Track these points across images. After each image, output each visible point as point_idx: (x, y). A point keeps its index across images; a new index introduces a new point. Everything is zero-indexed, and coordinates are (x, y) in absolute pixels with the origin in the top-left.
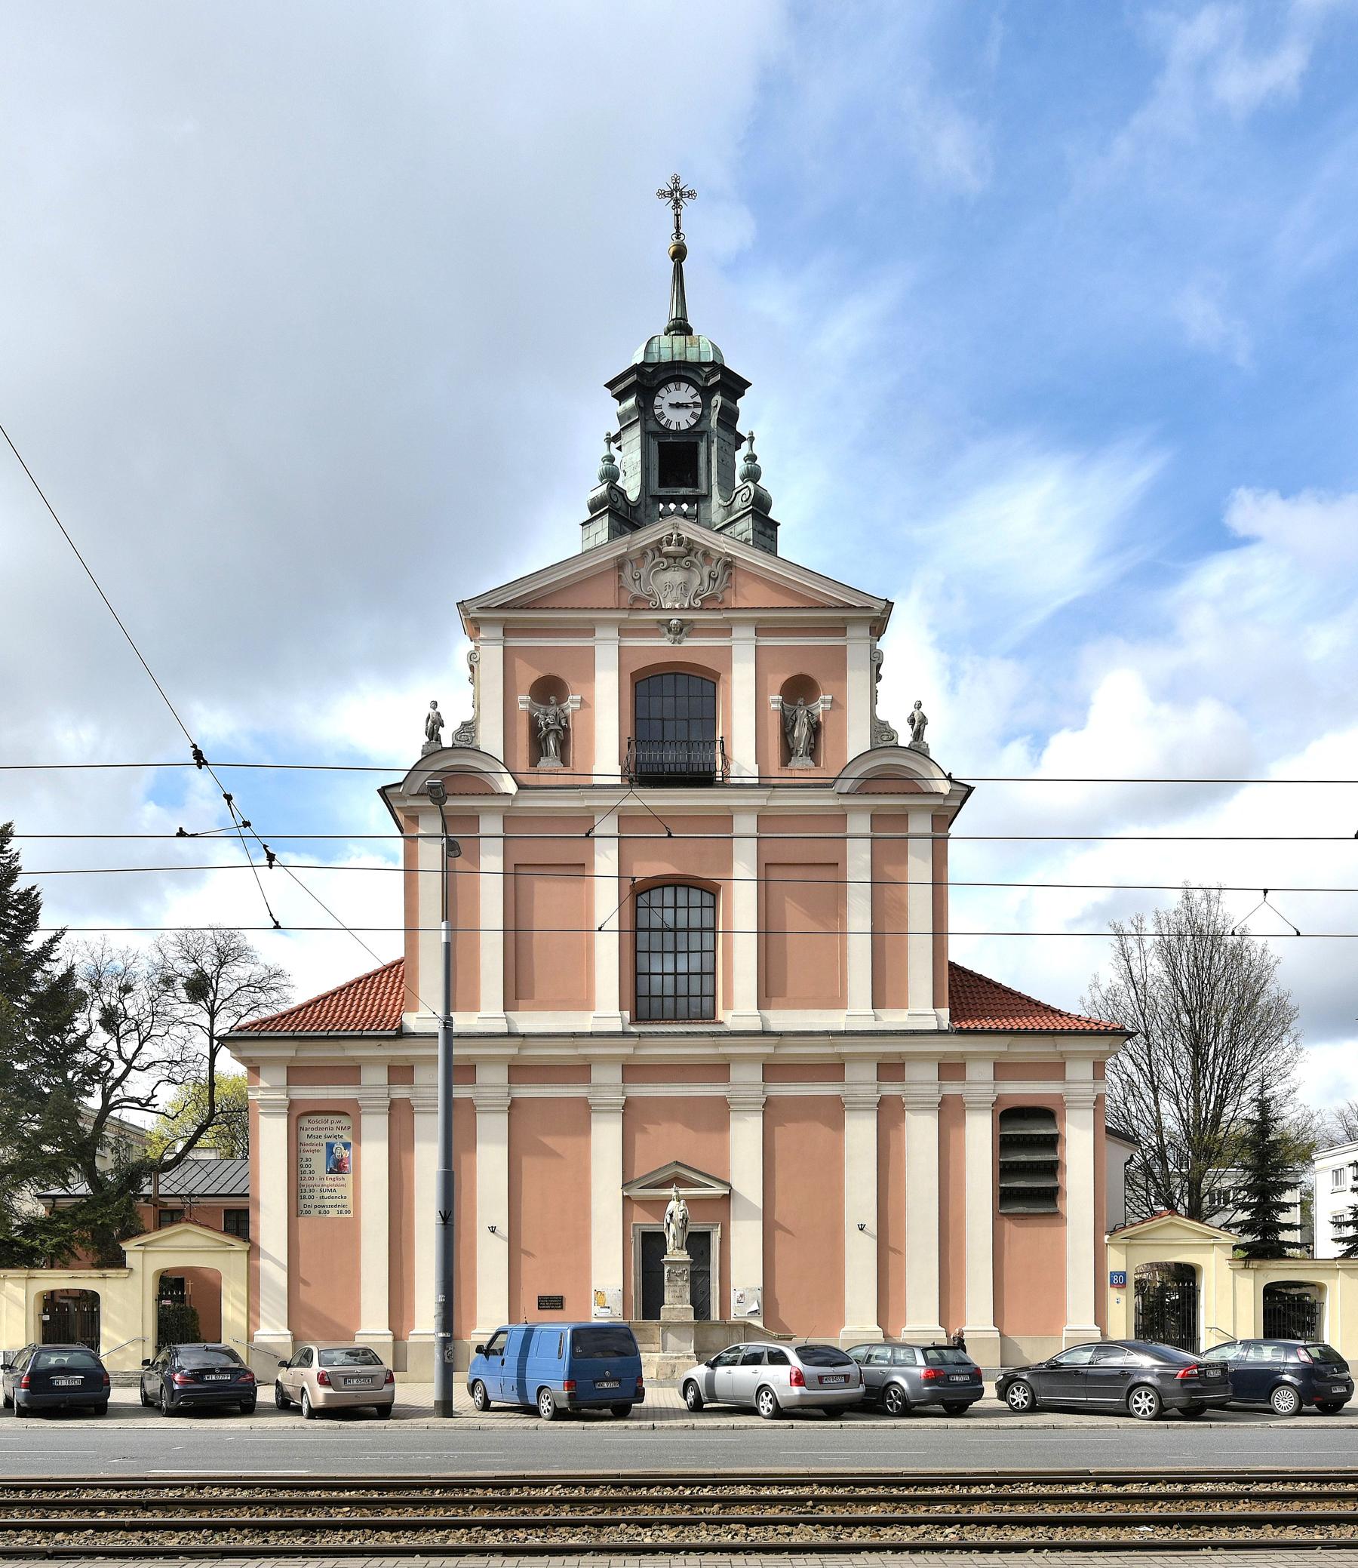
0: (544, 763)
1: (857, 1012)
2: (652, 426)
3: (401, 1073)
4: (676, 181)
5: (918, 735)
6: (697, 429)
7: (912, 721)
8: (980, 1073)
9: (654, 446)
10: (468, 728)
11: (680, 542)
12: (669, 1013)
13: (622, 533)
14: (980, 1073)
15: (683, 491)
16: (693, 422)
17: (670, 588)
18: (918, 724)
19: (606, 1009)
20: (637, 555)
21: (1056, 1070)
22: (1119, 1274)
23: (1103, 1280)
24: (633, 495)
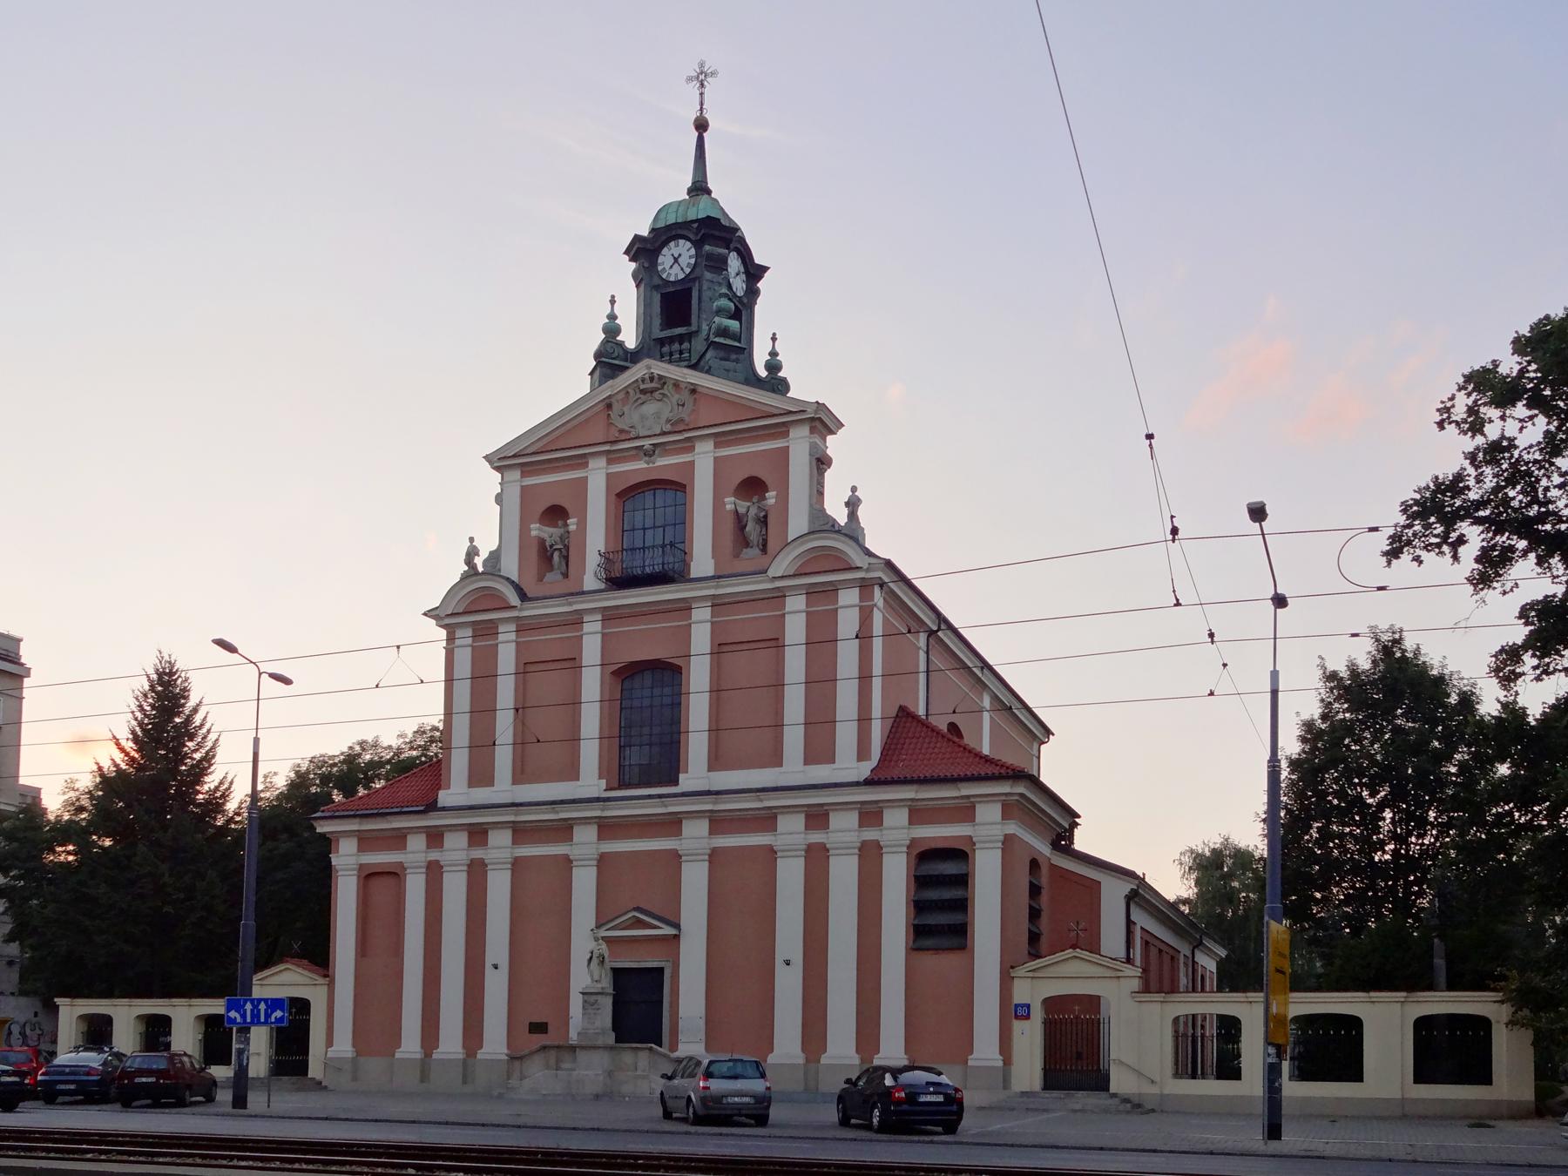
0: (549, 577)
1: (793, 769)
2: (656, 281)
3: (435, 837)
4: (702, 65)
5: (853, 516)
7: (847, 504)
8: (896, 819)
9: (657, 298)
10: (495, 557)
12: (636, 781)
14: (896, 819)
17: (651, 416)
18: (853, 504)
19: (591, 782)
20: (621, 396)
21: (965, 812)
22: (1022, 1006)
23: (1012, 1012)
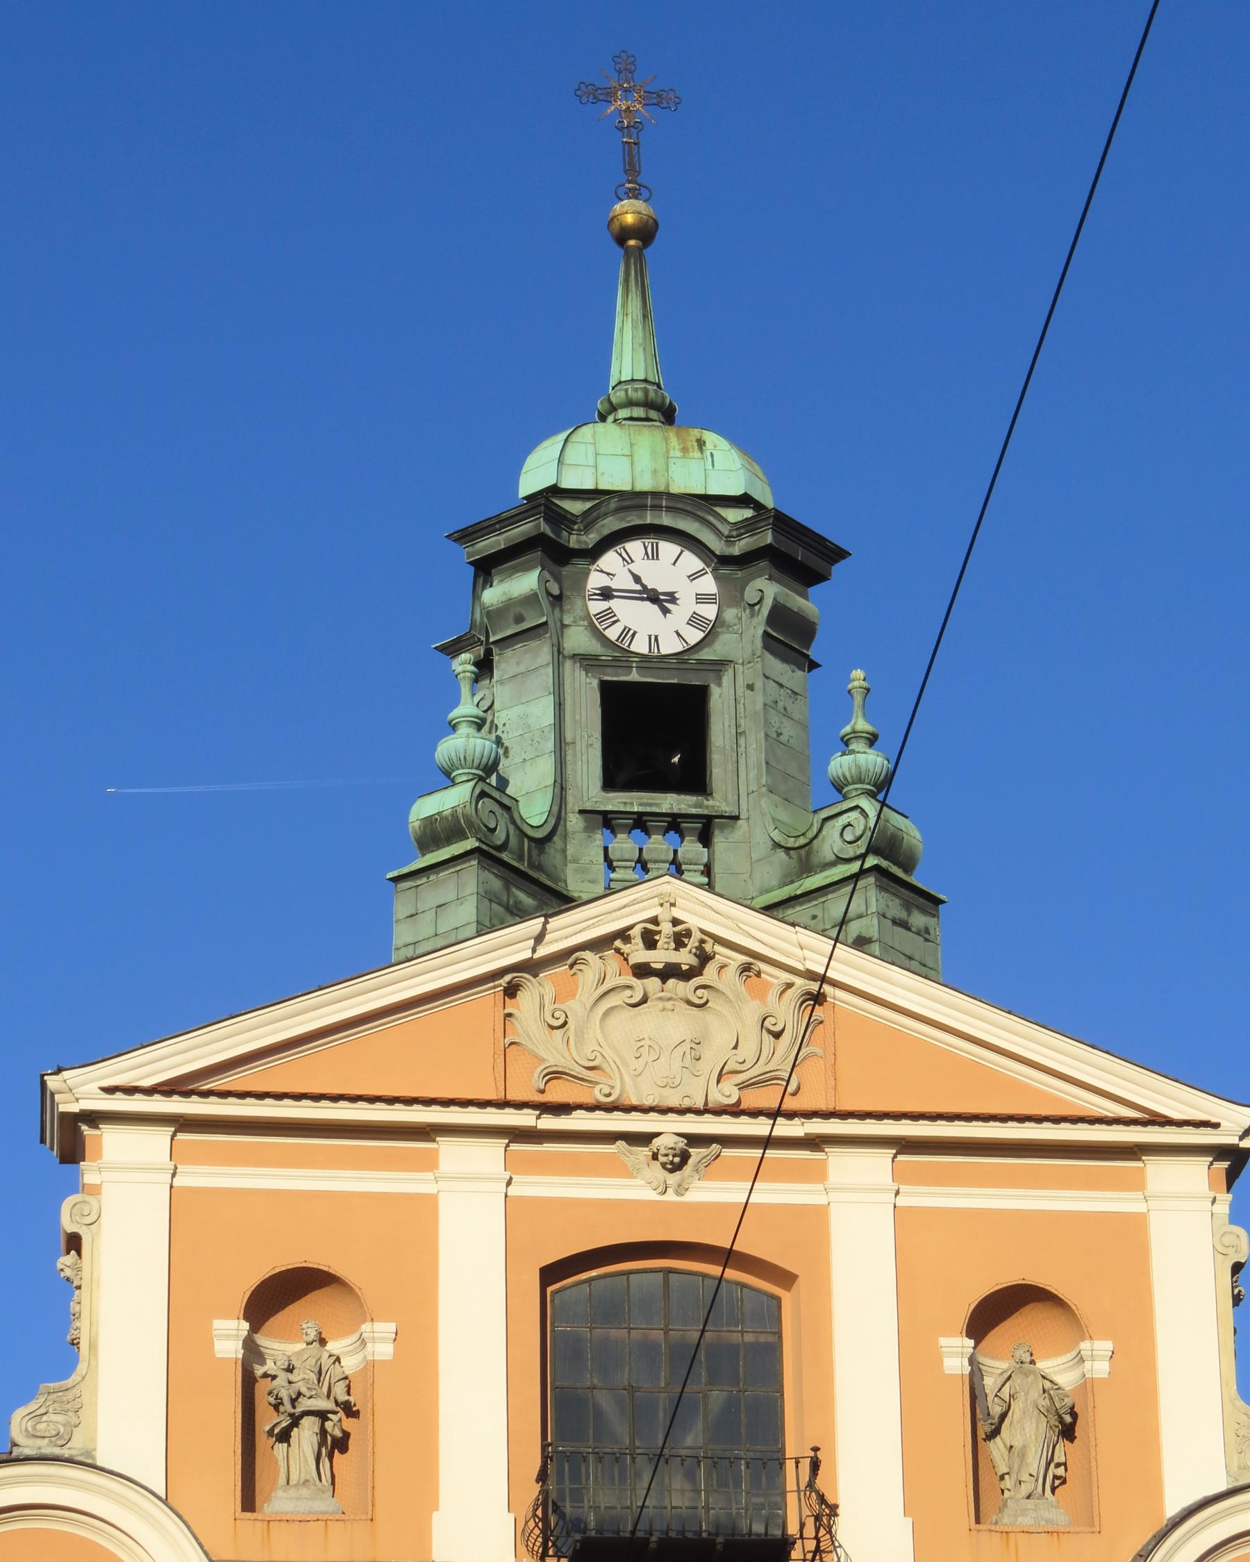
6: (706, 654)
11: (679, 941)
13: (519, 914)
15: (670, 802)
16: (694, 636)
24: (535, 812)
